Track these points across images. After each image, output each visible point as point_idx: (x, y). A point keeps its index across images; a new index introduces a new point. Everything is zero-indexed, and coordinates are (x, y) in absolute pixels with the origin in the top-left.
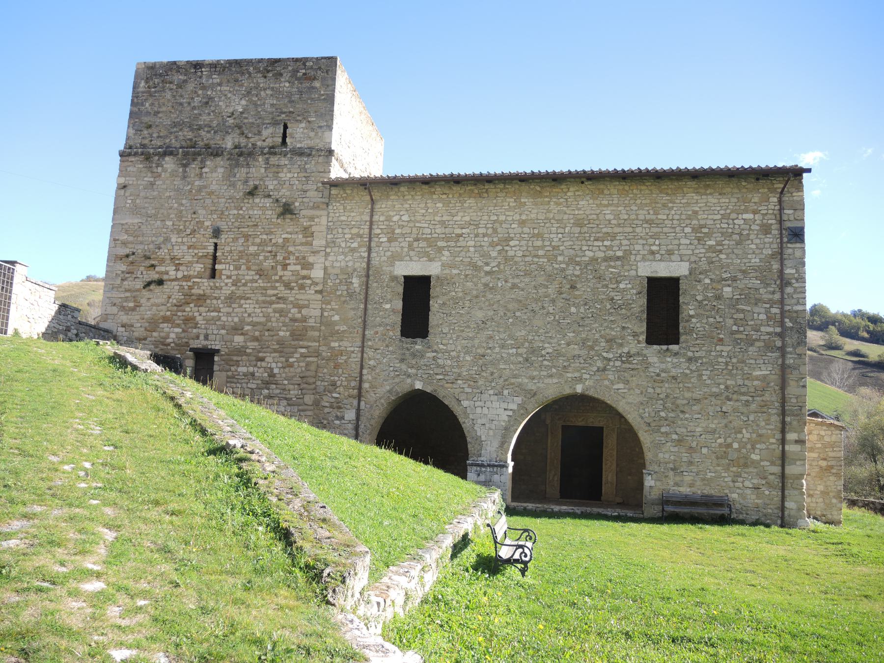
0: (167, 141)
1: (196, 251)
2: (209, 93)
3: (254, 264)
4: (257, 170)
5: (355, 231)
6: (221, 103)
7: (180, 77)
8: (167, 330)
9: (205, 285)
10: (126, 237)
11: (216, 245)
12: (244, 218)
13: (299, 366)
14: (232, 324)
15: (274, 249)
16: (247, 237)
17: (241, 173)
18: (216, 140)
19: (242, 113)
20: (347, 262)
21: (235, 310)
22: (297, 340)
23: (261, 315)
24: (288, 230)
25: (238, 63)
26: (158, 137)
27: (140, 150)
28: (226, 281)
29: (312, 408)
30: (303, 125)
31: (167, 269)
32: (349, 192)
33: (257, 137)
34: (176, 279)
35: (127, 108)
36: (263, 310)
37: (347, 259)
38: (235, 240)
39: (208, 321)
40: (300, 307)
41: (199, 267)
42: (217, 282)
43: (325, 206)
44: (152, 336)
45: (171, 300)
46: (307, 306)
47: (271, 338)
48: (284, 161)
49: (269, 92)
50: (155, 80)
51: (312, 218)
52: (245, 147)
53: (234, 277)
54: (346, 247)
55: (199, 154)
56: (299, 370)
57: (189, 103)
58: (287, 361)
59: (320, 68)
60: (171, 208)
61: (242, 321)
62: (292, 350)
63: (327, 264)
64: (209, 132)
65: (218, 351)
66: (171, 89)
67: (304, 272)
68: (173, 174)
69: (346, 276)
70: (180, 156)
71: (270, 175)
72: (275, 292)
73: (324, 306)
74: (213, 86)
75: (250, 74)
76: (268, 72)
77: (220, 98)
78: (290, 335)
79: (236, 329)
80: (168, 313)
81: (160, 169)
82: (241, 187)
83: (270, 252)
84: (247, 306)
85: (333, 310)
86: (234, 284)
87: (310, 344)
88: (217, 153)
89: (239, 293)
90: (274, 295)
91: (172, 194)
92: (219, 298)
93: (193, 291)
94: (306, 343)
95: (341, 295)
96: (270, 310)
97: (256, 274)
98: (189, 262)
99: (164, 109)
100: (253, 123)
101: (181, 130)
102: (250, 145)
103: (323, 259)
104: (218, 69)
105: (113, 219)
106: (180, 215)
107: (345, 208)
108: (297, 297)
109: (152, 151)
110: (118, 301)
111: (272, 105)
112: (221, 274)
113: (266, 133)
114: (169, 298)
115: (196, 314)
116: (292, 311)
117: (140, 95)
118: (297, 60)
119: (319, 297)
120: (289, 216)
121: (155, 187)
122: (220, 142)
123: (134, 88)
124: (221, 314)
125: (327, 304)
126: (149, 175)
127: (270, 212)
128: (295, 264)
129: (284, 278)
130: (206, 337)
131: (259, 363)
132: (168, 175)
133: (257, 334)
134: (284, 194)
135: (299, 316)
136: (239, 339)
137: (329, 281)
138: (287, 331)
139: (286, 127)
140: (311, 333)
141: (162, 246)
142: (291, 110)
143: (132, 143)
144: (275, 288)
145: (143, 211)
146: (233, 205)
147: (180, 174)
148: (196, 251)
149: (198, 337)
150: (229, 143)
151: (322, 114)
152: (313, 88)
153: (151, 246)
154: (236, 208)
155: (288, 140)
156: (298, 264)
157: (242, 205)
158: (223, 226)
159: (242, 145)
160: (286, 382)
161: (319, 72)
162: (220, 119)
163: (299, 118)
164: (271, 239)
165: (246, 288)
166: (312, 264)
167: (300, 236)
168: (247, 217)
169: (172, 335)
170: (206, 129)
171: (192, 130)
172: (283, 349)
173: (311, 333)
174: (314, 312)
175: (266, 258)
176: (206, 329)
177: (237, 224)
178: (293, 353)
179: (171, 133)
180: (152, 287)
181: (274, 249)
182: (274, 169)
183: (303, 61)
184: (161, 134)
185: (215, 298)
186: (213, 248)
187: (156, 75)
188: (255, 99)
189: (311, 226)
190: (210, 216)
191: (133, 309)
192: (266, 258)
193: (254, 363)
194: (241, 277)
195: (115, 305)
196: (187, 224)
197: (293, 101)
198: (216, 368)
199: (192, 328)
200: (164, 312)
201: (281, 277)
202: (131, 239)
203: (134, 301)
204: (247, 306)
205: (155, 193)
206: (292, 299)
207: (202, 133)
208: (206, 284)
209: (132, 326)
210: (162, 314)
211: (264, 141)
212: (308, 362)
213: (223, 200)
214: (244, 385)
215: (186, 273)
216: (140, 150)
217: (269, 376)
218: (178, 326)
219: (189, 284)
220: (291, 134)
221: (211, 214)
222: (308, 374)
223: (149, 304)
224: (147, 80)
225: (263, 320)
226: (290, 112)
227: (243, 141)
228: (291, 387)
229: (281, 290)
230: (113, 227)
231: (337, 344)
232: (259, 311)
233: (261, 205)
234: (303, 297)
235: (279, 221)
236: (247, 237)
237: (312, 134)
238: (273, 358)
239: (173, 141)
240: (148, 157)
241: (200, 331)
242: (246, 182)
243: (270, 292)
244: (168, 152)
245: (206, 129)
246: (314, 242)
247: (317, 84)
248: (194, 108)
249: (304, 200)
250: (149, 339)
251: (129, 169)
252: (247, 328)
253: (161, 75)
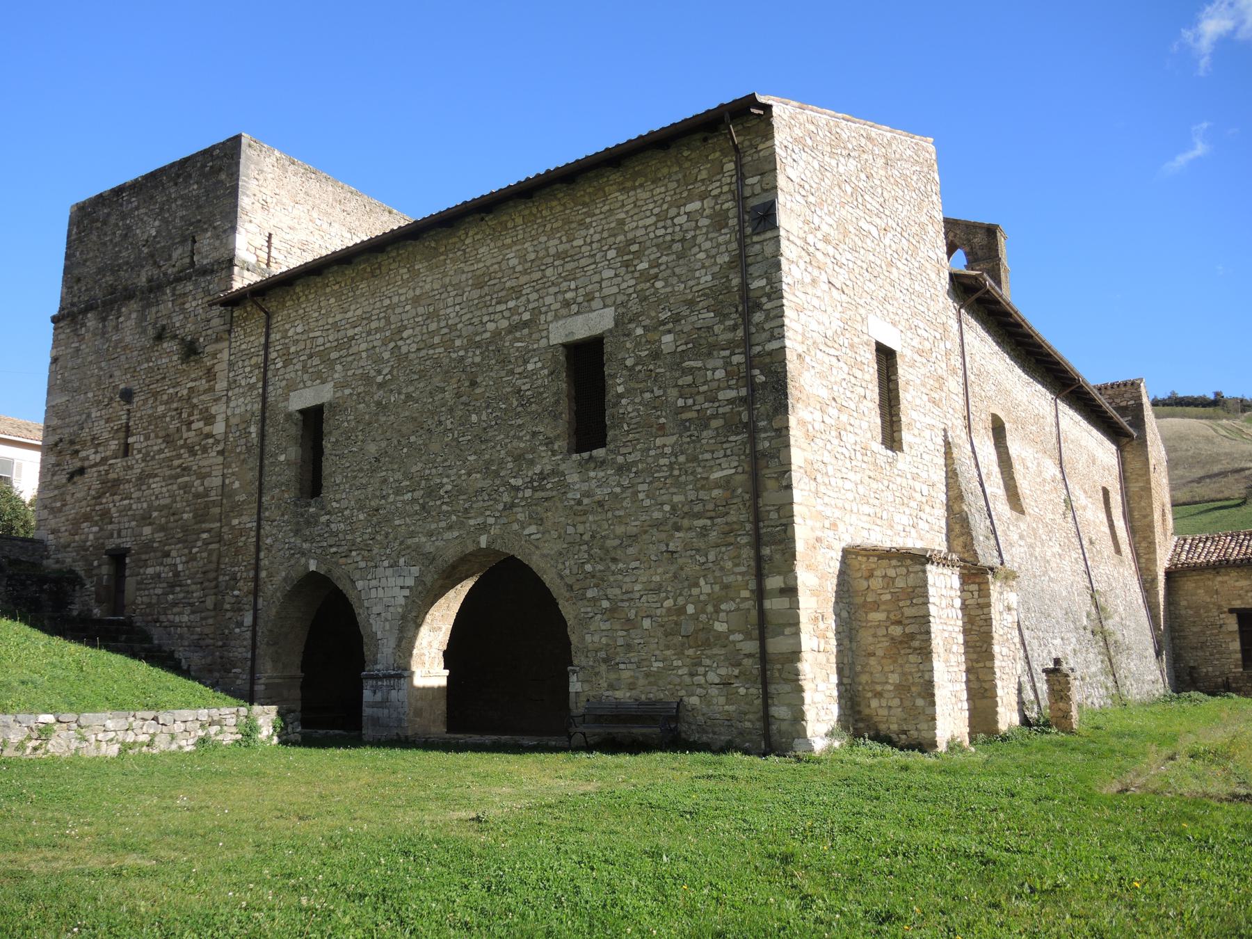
58: (190, 552)
61: (150, 507)
95: (240, 453)
96: (175, 487)
136: (147, 530)
169: (91, 537)
180: (75, 479)
217: (174, 576)
225: (168, 501)
236: (155, 395)
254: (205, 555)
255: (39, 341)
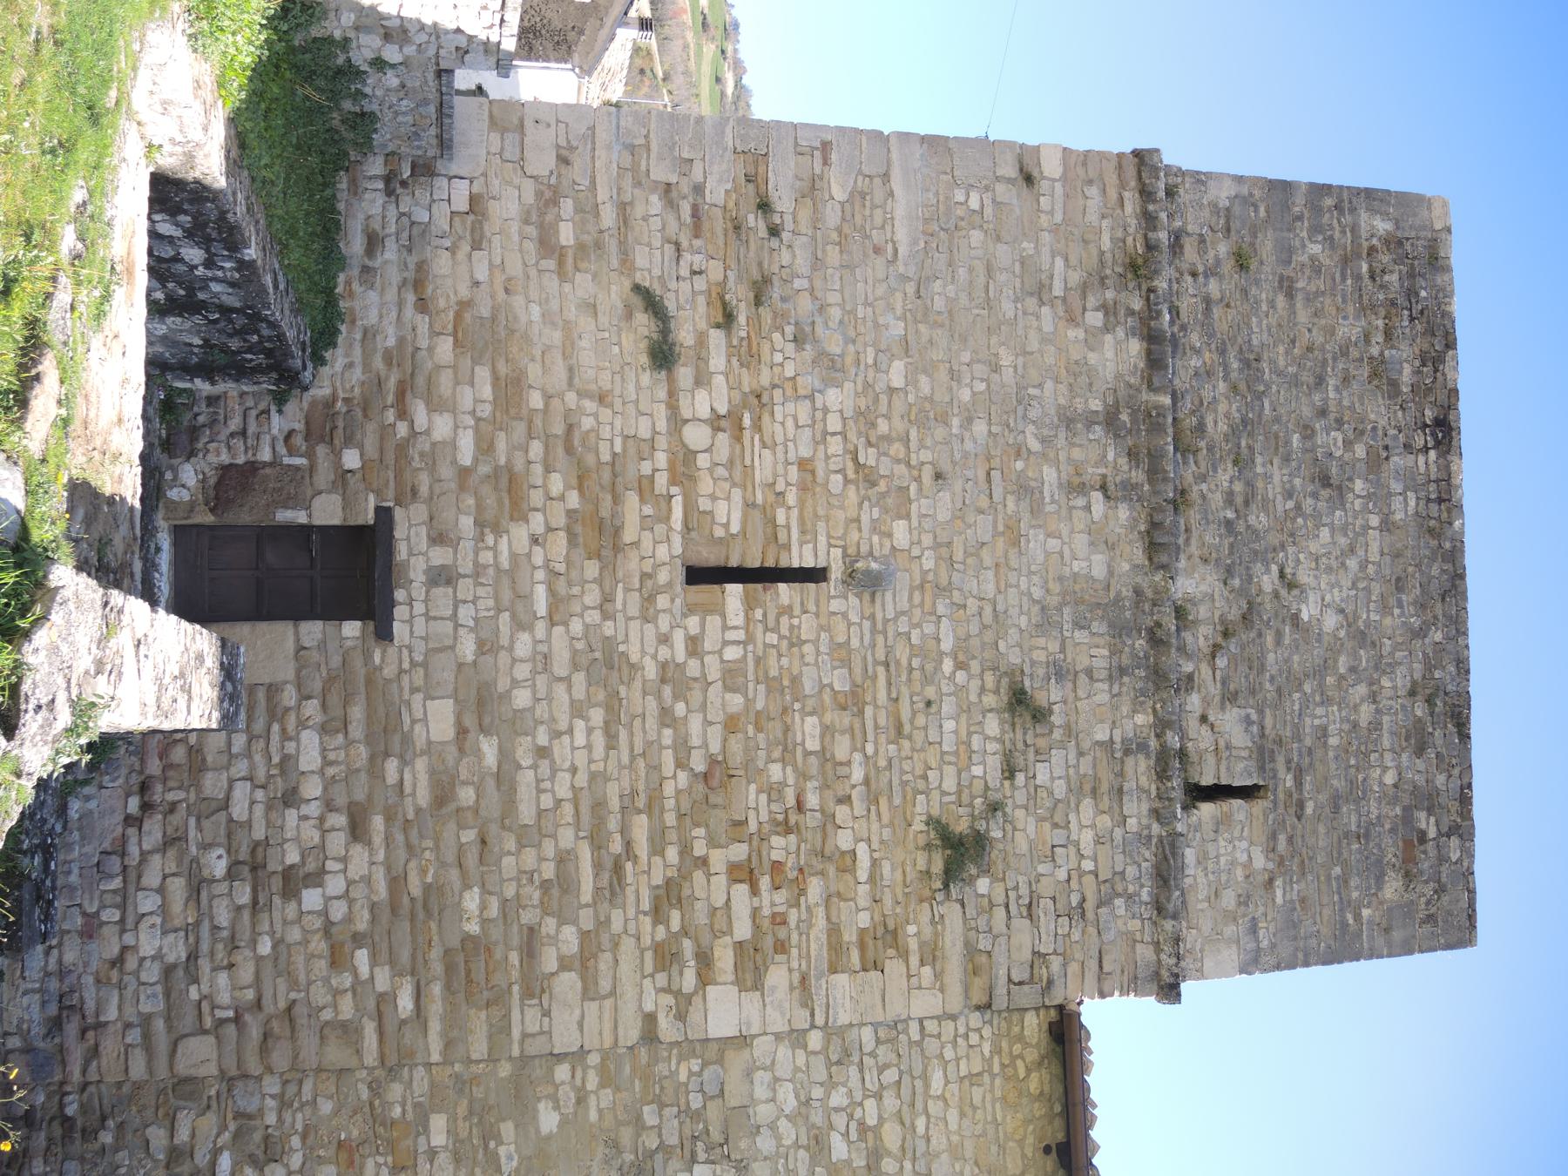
0: (1195, 338)
1: (791, 498)
2: (1359, 485)
3: (750, 750)
4: (1102, 713)
5: (891, 1136)
6: (1325, 533)
7: (1407, 370)
8: (466, 398)
9: (662, 551)
10: (839, 194)
11: (815, 575)
12: (927, 680)
13: (337, 993)
14: (503, 684)
15: (812, 820)
16: (853, 701)
17: (1091, 649)
18: (1203, 536)
19: (1295, 619)
20: (773, 1126)
21: (560, 690)
22: (450, 969)
23: (547, 801)
24: (886, 868)
25: (1454, 585)
26: (1208, 301)
27: (1163, 236)
28: (679, 638)
29: (162, 1072)
30: (1260, 861)
31: (719, 380)
32: (1033, 1085)
33: (1215, 690)
34: (677, 421)
35: (1303, 170)
36: (568, 809)
37: (783, 1124)
38: (842, 654)
39: (512, 574)
40: (583, 962)
41: (728, 514)
42: (674, 597)
43: (978, 997)
44: (434, 334)
45: (590, 406)
46: (589, 992)
47: (450, 857)
48: (1137, 812)
49: (1365, 713)
50: (1394, 269)
51: (931, 954)
52: (1182, 649)
53: (693, 668)
54: (828, 1112)
55: (1155, 473)
56: (320, 995)
57: (1323, 413)
58: (358, 940)
59: (1441, 890)
60: (954, 375)
61: (518, 723)
62: (405, 956)
63: (762, 1046)
64: (1229, 498)
65: (384, 634)
66: (1367, 337)
67: (724, 958)
68: (1078, 373)
69: (716, 1136)
70: (1145, 396)
71: (1085, 766)
72: (642, 848)
73: (594, 1059)
74: (1379, 498)
75: (1421, 633)
76: (1430, 701)
77: (1344, 530)
78: (467, 938)
79: (481, 703)
80: (536, 400)
81: (1095, 319)
82: (1040, 656)
83: (800, 806)
84: (580, 740)
85: (581, 1101)
86: (668, 673)
87: (435, 1027)
88: (1158, 545)
89: (632, 695)
90: (628, 844)
91: (1008, 375)
92: (607, 616)
93: (632, 499)
94: (436, 1008)
95: (639, 1124)
96: (567, 837)
97: (713, 762)
98: (748, 470)
99: (1303, 316)
100: (1262, 668)
101: (1234, 388)
102: (1188, 667)
103: (780, 1026)
104: (1434, 507)
105: (905, 137)
106: (927, 415)
107: (973, 1079)
108: (628, 944)
109: (1161, 284)
110: (577, 173)
111: (1323, 733)
112: (705, 610)
113: (1230, 722)
114: (602, 399)
115: (537, 523)
116: (569, 935)
117: (1348, 219)
118: (1465, 799)
119: (631, 1032)
120: (938, 866)
121: (1031, 303)
122: (1194, 548)
123: (1369, 194)
124: (540, 629)
125: (602, 1069)
126: (1075, 278)
127: (950, 784)
128: (755, 912)
129: (698, 876)
130: (442, 577)
131: (339, 820)
132: (1075, 356)
133: (467, 795)
134: (1023, 832)
135: (549, 961)
136: (438, 720)
137: (695, 1065)
138: (484, 922)
139: (1247, 793)
140: (479, 1022)
141: (809, 352)
142: (1309, 810)
143: (1184, 196)
144: (657, 849)
145: (941, 259)
146: (974, 628)
147: (1079, 404)
148: (791, 498)
149: (439, 538)
150: (1193, 582)
151: (1295, 926)
152: (1380, 880)
153: (805, 305)
154: (962, 642)
155: (1207, 809)
156: (756, 927)
157: (975, 666)
158: (891, 602)
159: (1187, 636)
160: (265, 947)
161: (1428, 890)
162: (1274, 539)
163: (1282, 838)
164: (846, 800)
165: (651, 723)
166: (758, 986)
167: (864, 920)
168: (930, 692)
169: (442, 427)
170: (1238, 487)
171: (1234, 432)
172: (408, 913)
173: (479, 1022)
174: (570, 1021)
175: (774, 791)
176: (478, 571)
177: (902, 653)
178: (392, 962)
179: (1222, 352)
180: (642, 319)
181: (812, 820)
182: (1106, 778)
183: (1462, 829)
184: (1217, 312)
185: (608, 598)
186: (809, 563)
187: (1412, 275)
188: (1343, 664)
189: (904, 955)
190: (927, 540)
191: (547, 244)
192: (774, 791)
193: (341, 800)
194: (696, 696)
195: (563, 161)
196: (897, 449)
197: (1336, 809)
198: (312, 630)
199: (480, 507)
200: (542, 378)
201: (704, 861)
202: (832, 216)
203: (581, 248)
204: (580, 740)
205: (1008, 308)
206: (617, 925)
207: (1225, 475)
208: (662, 552)
209: (476, 246)
210: (534, 372)
211: (1204, 719)
212: (359, 1031)
213: (990, 589)
214: (241, 768)
215: (703, 461)
216: (1163, 236)
217: (288, 873)
218: (485, 447)
219: (662, 480)
220: (1220, 824)
221: (937, 546)
222: (308, 1041)
223: (572, 313)
224: (1394, 242)
225: (526, 814)
226: (1301, 805)
227: (1201, 637)
228: (246, 973)
229: (649, 873)
230: (878, 135)
231: (439, 1139)
232: (563, 791)
233: (976, 742)
234: (626, 968)
235: (918, 826)
236: (853, 701)
237: (1229, 900)
238: (368, 880)
239: (1195, 362)
240: (1138, 269)
241: (467, 546)
242: (1060, 672)
243: (641, 827)
244: (1158, 350)
245: (1238, 487)
246: (842, 979)
247: (1392, 888)
248: (1308, 433)
249: (1000, 913)
250: (423, 323)
251: (1093, 191)
252: (489, 750)
253: (1411, 293)
254: (347, 1008)
255: (1074, 110)
